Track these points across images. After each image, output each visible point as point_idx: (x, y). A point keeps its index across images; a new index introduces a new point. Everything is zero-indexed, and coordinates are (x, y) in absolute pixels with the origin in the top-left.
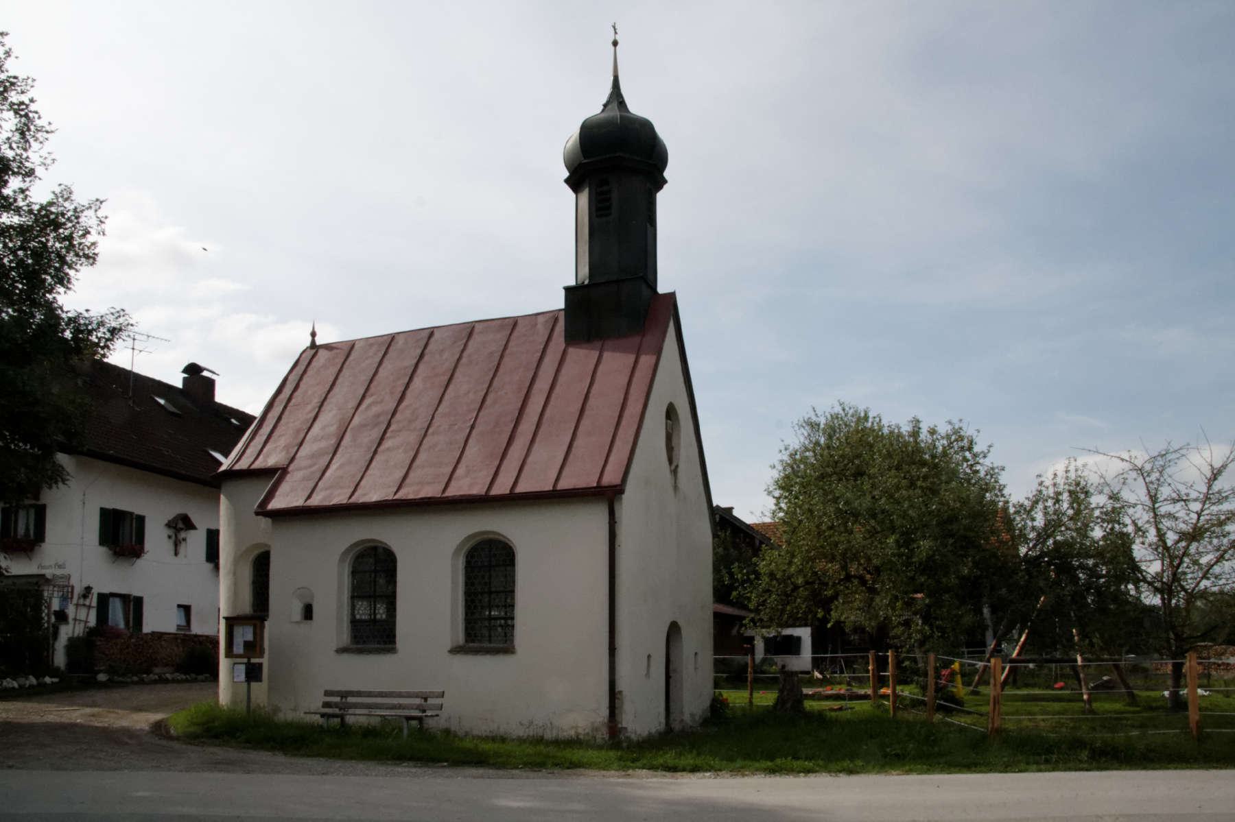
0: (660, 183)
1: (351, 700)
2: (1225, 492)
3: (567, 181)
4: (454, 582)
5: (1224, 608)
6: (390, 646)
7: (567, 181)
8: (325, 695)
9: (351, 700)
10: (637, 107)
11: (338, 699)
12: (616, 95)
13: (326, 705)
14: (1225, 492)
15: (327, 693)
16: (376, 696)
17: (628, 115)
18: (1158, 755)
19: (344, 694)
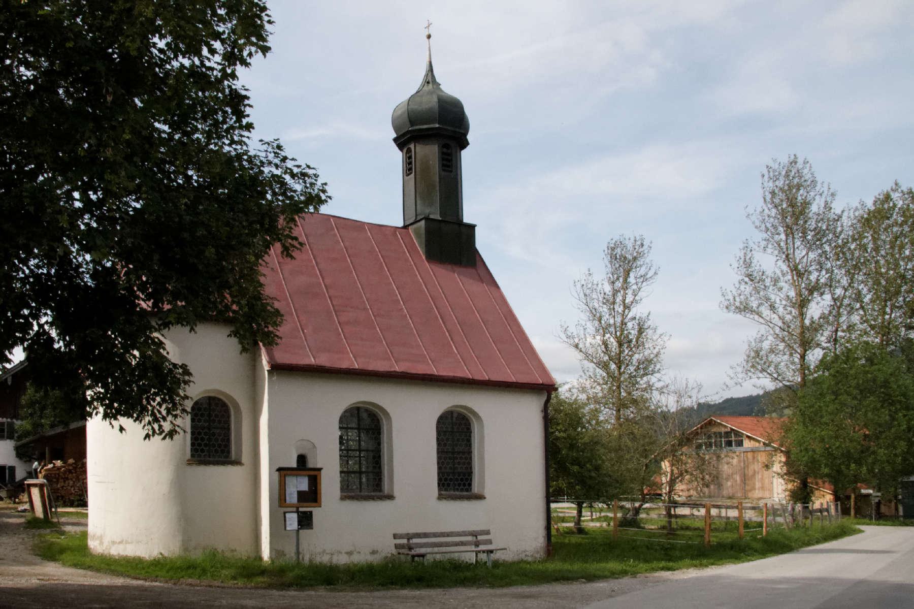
0: (464, 144)
1: (415, 541)
2: (263, 261)
3: (395, 140)
4: (482, 458)
5: (897, 452)
6: (79, 510)
7: (395, 140)
8: (395, 538)
9: (415, 541)
10: (450, 87)
11: (469, 538)
12: (430, 78)
13: (397, 546)
14: (263, 261)
15: (395, 536)
16: (439, 536)
17: (443, 94)
18: (343, 599)
19: (409, 537)
